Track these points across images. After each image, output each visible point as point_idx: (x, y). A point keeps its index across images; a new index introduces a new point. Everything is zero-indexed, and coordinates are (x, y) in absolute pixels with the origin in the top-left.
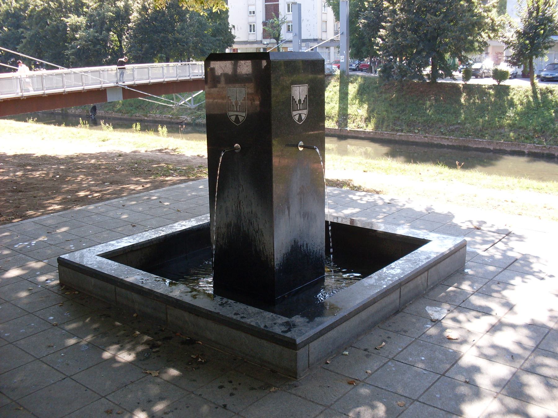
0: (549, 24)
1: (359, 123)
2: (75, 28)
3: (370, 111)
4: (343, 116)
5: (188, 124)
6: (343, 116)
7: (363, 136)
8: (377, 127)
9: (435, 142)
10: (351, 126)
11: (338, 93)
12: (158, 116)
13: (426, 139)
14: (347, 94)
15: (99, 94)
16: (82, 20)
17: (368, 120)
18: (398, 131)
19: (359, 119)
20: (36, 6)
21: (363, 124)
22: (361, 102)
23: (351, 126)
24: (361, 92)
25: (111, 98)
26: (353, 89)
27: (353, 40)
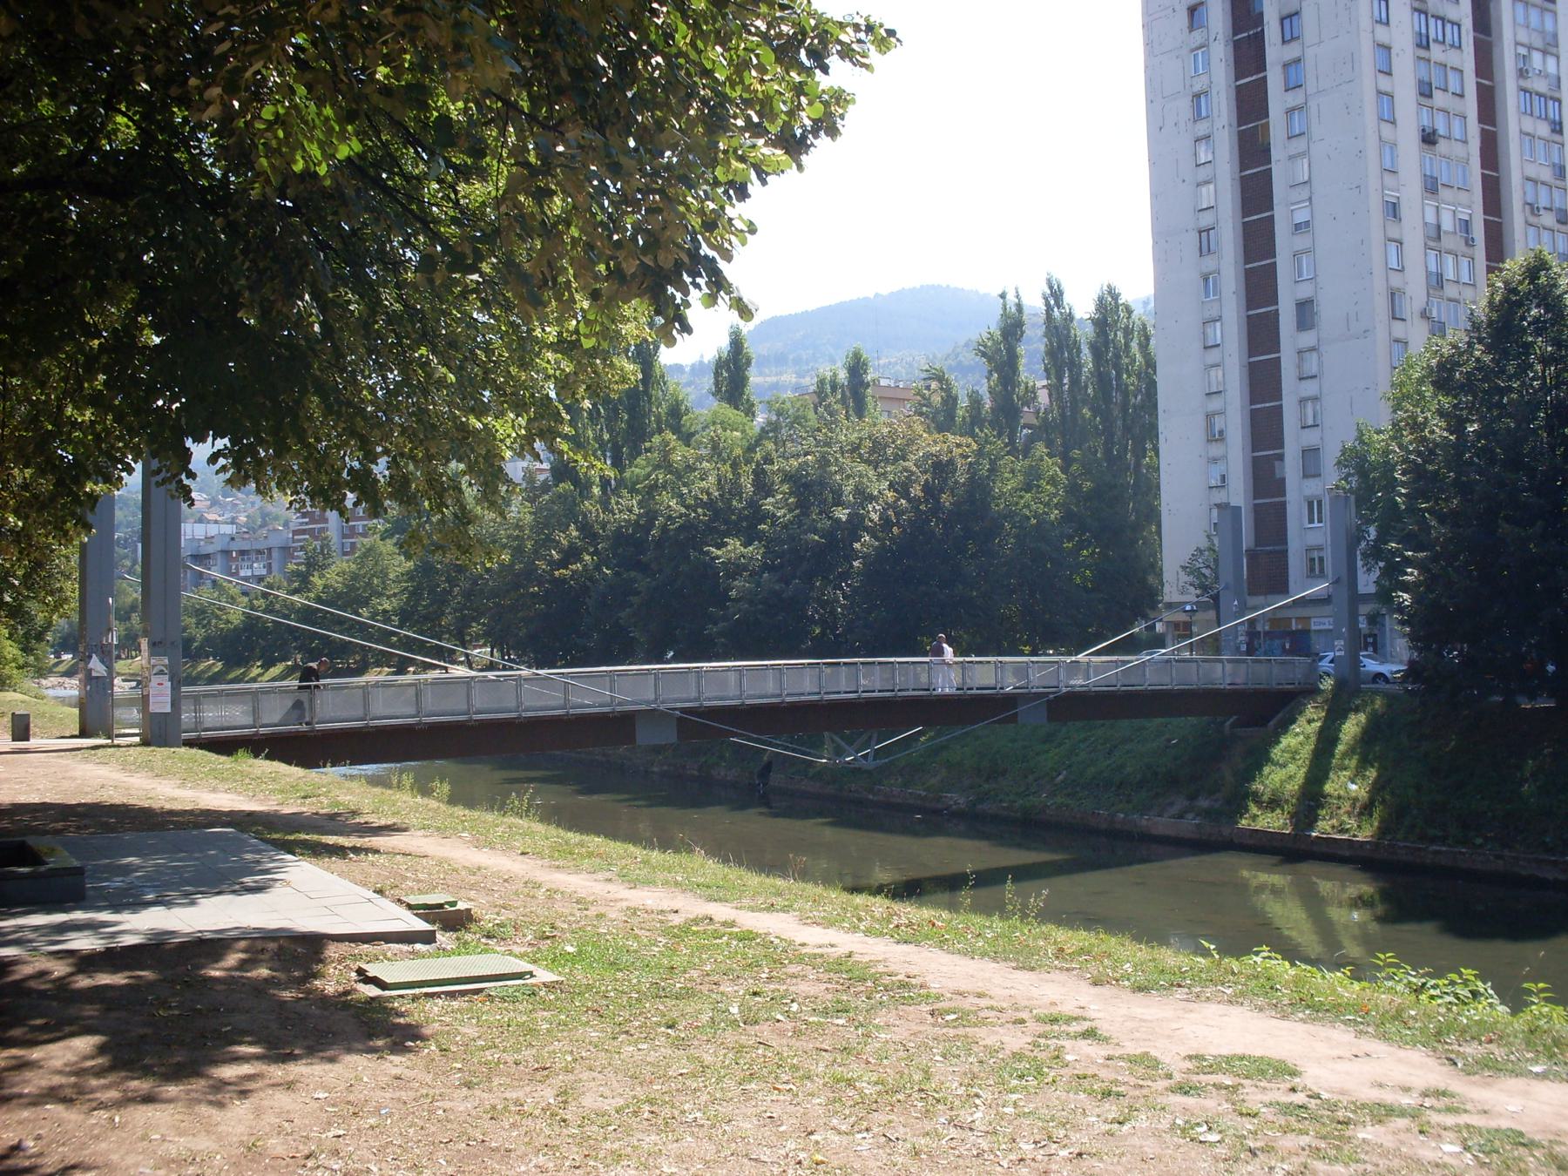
0: (514, 370)
1: (1345, 818)
2: (735, 569)
3: (1377, 788)
4: (1311, 799)
5: (959, 815)
6: (1311, 799)
7: (1347, 854)
8: (1383, 831)
9: (1524, 873)
10: (1324, 827)
11: (1313, 739)
12: (896, 790)
13: (1501, 862)
14: (1335, 741)
15: (615, 726)
16: (755, 551)
17: (1366, 810)
18: (1433, 840)
19: (1346, 806)
20: (670, 518)
21: (1352, 823)
22: (1364, 763)
23: (1324, 827)
24: (1367, 739)
25: (645, 736)
26: (1351, 727)
27: (749, 524)
